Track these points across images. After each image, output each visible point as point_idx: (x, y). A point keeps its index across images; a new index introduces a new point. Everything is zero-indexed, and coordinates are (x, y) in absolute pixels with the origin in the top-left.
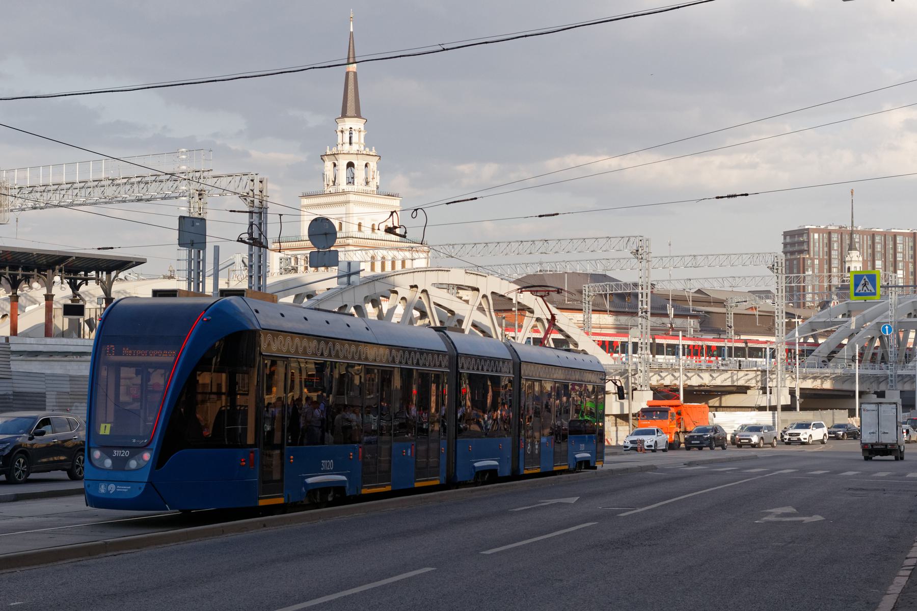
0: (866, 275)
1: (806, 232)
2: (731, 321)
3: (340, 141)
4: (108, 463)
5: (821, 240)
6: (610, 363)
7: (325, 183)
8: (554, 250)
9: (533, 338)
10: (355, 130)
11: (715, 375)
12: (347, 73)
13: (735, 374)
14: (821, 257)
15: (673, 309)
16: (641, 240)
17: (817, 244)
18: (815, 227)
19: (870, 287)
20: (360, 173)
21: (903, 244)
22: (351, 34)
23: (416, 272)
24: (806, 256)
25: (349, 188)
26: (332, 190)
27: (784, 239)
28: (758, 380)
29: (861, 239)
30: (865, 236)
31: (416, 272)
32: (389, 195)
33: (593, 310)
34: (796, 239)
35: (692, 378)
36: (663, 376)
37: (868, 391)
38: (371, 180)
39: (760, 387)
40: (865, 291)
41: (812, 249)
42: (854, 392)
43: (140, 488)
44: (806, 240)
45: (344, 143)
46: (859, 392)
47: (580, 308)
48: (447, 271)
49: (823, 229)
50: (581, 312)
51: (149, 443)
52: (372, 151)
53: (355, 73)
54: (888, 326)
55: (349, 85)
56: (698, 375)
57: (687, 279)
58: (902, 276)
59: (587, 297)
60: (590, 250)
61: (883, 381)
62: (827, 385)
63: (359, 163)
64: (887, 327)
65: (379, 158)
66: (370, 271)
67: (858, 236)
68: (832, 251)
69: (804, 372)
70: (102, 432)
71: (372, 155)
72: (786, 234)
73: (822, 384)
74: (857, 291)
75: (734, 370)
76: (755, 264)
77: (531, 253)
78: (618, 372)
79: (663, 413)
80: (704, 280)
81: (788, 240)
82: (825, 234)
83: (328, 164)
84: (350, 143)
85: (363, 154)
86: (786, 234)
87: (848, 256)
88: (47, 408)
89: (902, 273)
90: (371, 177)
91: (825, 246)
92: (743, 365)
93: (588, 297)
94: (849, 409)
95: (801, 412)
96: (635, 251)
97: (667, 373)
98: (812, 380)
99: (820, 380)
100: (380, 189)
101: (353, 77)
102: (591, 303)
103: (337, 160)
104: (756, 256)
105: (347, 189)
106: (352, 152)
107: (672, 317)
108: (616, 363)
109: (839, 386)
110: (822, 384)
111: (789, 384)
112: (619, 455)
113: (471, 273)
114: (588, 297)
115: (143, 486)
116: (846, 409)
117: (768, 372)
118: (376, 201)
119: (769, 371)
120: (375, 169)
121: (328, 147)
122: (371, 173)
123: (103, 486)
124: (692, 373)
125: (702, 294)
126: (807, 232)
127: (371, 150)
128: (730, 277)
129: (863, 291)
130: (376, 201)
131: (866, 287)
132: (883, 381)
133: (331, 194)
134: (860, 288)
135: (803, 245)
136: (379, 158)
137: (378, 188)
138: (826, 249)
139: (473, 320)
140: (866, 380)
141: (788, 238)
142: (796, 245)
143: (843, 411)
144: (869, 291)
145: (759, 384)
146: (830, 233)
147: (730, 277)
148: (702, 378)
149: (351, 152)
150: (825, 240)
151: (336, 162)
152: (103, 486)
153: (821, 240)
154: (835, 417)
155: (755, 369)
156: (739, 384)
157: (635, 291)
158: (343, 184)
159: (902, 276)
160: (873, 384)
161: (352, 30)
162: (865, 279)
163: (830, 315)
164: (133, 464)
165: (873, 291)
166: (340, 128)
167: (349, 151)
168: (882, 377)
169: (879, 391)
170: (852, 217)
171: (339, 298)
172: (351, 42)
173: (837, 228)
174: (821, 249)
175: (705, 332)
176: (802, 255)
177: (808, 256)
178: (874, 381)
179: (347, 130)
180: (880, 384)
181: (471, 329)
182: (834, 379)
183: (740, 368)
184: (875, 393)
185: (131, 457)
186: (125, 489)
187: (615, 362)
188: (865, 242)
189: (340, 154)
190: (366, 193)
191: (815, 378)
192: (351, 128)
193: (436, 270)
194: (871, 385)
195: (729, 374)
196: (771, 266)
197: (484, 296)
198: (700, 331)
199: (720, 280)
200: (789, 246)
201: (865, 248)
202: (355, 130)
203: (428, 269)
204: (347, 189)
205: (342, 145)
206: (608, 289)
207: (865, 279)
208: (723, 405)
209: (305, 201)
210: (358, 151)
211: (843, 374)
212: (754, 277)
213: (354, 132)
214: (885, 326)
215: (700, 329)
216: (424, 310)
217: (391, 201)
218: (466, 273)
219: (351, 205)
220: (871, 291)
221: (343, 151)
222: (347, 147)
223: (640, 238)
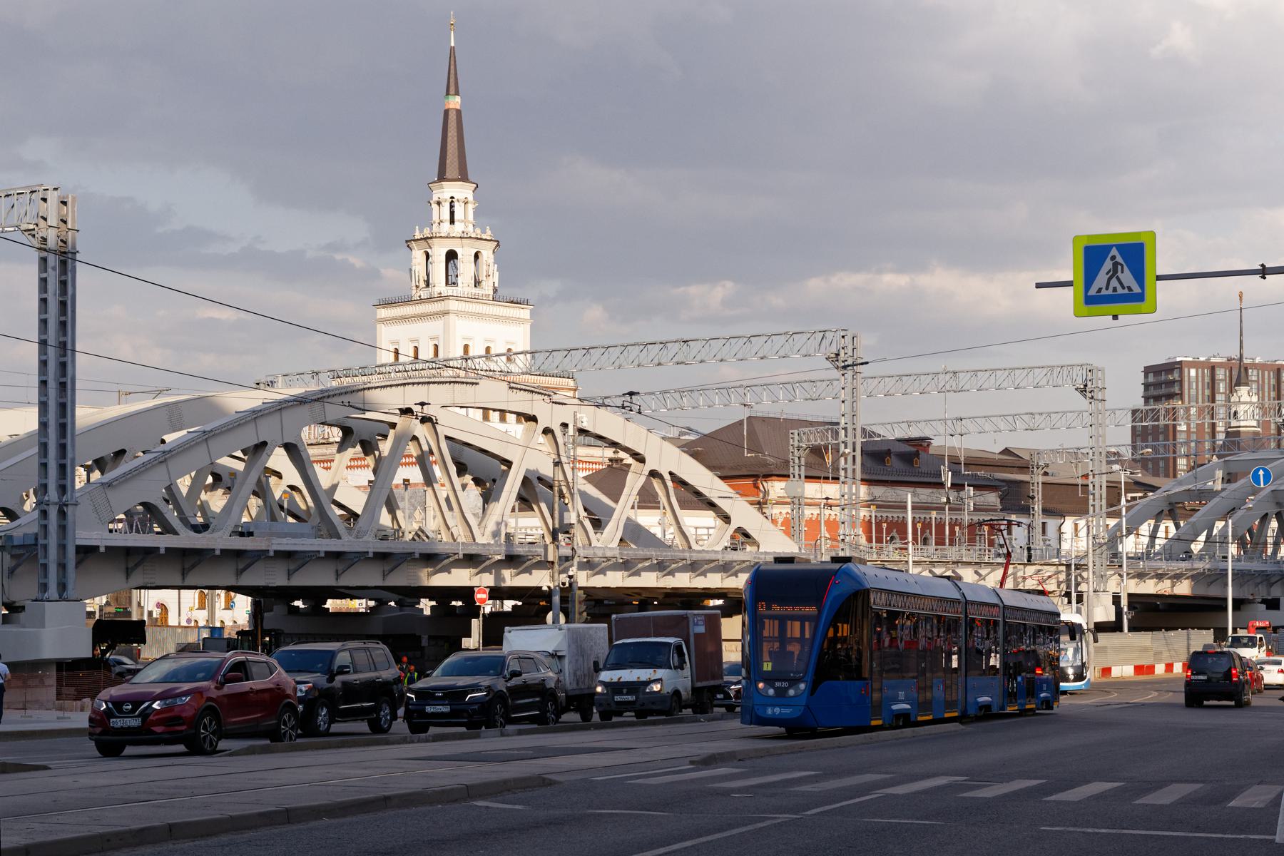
0: (1116, 246)
2: (1038, 493)
3: (435, 218)
4: (771, 692)
5: (1200, 379)
8: (699, 358)
9: (1130, 595)
10: (458, 201)
11: (983, 572)
12: (447, 112)
13: (1020, 570)
15: (950, 473)
16: (843, 337)
17: (1194, 384)
18: (1190, 359)
19: (1127, 277)
20: (465, 267)
22: (452, 49)
23: (409, 384)
24: (1177, 402)
25: (450, 291)
26: (424, 295)
28: (1061, 580)
29: (1260, 376)
30: (1266, 373)
31: (409, 384)
32: (512, 302)
33: (806, 477)
34: (1163, 378)
37: (1251, 598)
38: (484, 278)
39: (1064, 592)
40: (1115, 289)
41: (1186, 392)
42: (1226, 599)
43: (800, 710)
44: (1177, 378)
45: (442, 222)
46: (1234, 600)
47: (785, 473)
48: (473, 384)
49: (1203, 362)
51: (803, 677)
52: (485, 233)
53: (458, 112)
54: (1264, 470)
55: (449, 129)
57: (957, 419)
59: (796, 451)
60: (759, 355)
61: (1276, 582)
62: (1184, 588)
63: (465, 253)
64: (1261, 473)
65: (496, 243)
66: (482, 420)
67: (1255, 372)
68: (1217, 395)
69: (1141, 567)
70: (765, 669)
71: (486, 240)
72: (1148, 370)
73: (1173, 586)
74: (1092, 292)
75: (1019, 564)
77: (659, 364)
81: (1151, 379)
82: (1206, 370)
83: (418, 255)
84: (452, 221)
85: (470, 237)
86: (1148, 370)
87: (1235, 394)
91: (1206, 386)
93: (799, 450)
94: (1215, 629)
95: (1130, 634)
96: (833, 356)
98: (1155, 580)
100: (500, 293)
101: (455, 117)
103: (431, 248)
104: (1056, 370)
105: (446, 292)
107: (949, 486)
109: (1203, 591)
110: (1173, 586)
111: (1113, 585)
112: (688, 723)
113: (521, 390)
114: (799, 450)
115: (802, 708)
116: (1209, 629)
117: (1073, 567)
118: (491, 311)
119: (1075, 565)
120: (491, 261)
122: (485, 268)
123: (770, 709)
124: (941, 567)
125: (1010, 455)
127: (484, 232)
128: (1026, 414)
129: (1110, 292)
132: (1276, 582)
133: (421, 300)
136: (496, 243)
137: (495, 290)
138: (1207, 392)
140: (1248, 581)
141: (1151, 375)
142: (1163, 386)
143: (1204, 632)
144: (1126, 291)
145: (1063, 586)
146: (1213, 368)
147: (1026, 414)
151: (429, 251)
152: (770, 709)
153: (1200, 379)
154: (1191, 642)
155: (1055, 561)
157: (872, 439)
158: (439, 284)
160: (1260, 586)
162: (1113, 258)
163: (1196, 478)
164: (791, 692)
165: (1137, 289)
166: (435, 198)
167: (449, 234)
168: (1274, 575)
169: (1270, 598)
170: (1241, 335)
173: (1224, 360)
174: (1200, 392)
175: (1008, 512)
176: (1171, 400)
177: (1180, 402)
178: (1261, 582)
179: (446, 200)
180: (1271, 586)
182: (1193, 578)
184: (1264, 601)
185: (790, 687)
186: (788, 711)
188: (1266, 381)
189: (436, 237)
190: (474, 299)
191: (1160, 577)
192: (452, 198)
193: (450, 382)
194: (1257, 589)
196: (1082, 387)
197: (547, 431)
198: (1001, 510)
199: (1010, 419)
201: (1266, 390)
202: (458, 201)
203: (432, 380)
204: (446, 292)
207: (1113, 258)
209: (383, 313)
210: (463, 232)
211: (1209, 570)
212: (1065, 413)
213: (456, 204)
214: (1258, 470)
218: (510, 388)
219: (452, 317)
220: (1130, 289)
221: (439, 233)
222: (446, 228)
223: (843, 333)
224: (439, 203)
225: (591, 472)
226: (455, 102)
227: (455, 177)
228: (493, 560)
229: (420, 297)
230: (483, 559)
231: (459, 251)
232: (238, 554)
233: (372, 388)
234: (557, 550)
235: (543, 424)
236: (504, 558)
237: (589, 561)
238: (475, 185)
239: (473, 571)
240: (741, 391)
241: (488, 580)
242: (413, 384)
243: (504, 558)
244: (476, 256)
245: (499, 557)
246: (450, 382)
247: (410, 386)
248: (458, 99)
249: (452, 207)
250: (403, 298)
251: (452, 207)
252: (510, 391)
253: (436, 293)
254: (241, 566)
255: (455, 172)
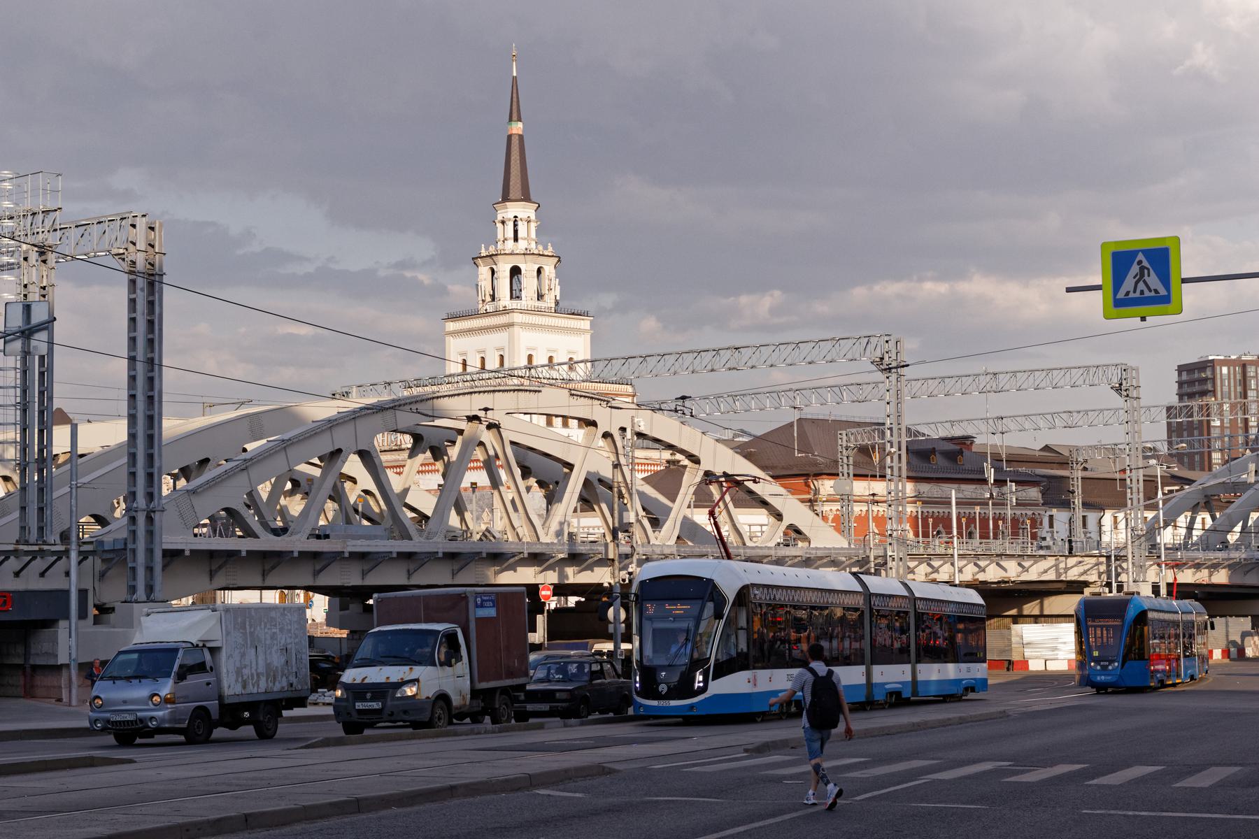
1: (1209, 364)
2: (1078, 488)
3: (500, 236)
5: (1232, 376)
6: (818, 546)
7: (480, 298)
8: (750, 364)
10: (521, 219)
12: (510, 137)
15: (993, 470)
16: (887, 342)
17: (1226, 381)
18: (1222, 358)
19: (1153, 280)
20: (529, 283)
22: (515, 79)
23: (475, 392)
25: (515, 304)
26: (490, 307)
27: (1179, 376)
31: (475, 392)
32: (573, 314)
34: (1196, 375)
35: (987, 569)
36: (982, 566)
38: (547, 292)
39: (1104, 583)
40: (1142, 292)
41: (1219, 389)
44: (1210, 376)
48: (536, 391)
49: (1234, 360)
50: (866, 478)
52: (547, 249)
53: (521, 137)
56: (998, 564)
59: (844, 451)
62: (1221, 577)
63: (528, 268)
66: (545, 425)
68: (1249, 392)
69: (1179, 557)
72: (1181, 369)
73: (1210, 576)
74: (1121, 295)
75: (1061, 556)
76: (1091, 383)
78: (853, 561)
79: (1161, 609)
80: (1024, 418)
81: (1185, 377)
82: (1237, 368)
83: (484, 271)
84: (516, 239)
85: (533, 254)
86: (1181, 369)
90: (547, 288)
92: (1077, 547)
93: (847, 449)
94: (1253, 617)
96: (878, 360)
97: (942, 562)
98: (1193, 570)
99: (1207, 571)
101: (518, 142)
102: (851, 459)
103: (496, 264)
104: (1092, 370)
106: (517, 252)
107: (992, 482)
108: (852, 546)
109: (1239, 580)
110: (1210, 576)
113: (581, 396)
114: (847, 449)
116: (1247, 616)
118: (569, 324)
119: (1115, 556)
120: (553, 275)
121: (483, 245)
126: (1211, 364)
127: (546, 248)
128: (1065, 412)
129: (1137, 294)
130: (569, 324)
131: (1145, 282)
133: (487, 314)
134: (1129, 283)
135: (1206, 384)
137: (557, 303)
138: (1239, 389)
139: (588, 472)
141: (1184, 374)
142: (1197, 383)
143: (1242, 619)
144: (1153, 294)
146: (1244, 366)
147: (1065, 412)
148: (1005, 570)
149: (515, 252)
150: (1238, 375)
151: (494, 267)
153: (1232, 376)
154: (1230, 630)
156: (1068, 579)
157: (917, 438)
161: (515, 74)
162: (1140, 262)
165: (1163, 292)
166: (500, 218)
167: (513, 251)
171: (327, 436)
172: (515, 91)
174: (1232, 389)
175: (1050, 506)
176: (1205, 397)
179: (510, 220)
181: (673, 501)
182: (1230, 567)
183: (1070, 553)
187: (849, 544)
189: (501, 254)
190: (537, 311)
191: (1198, 567)
192: (516, 217)
195: (1051, 561)
196: (1117, 385)
197: (606, 435)
198: (1043, 504)
200: (1186, 386)
202: (521, 219)
204: (510, 305)
205: (504, 242)
206: (876, 436)
207: (1140, 262)
208: (1046, 613)
209: (451, 326)
210: (526, 249)
211: (1245, 559)
212: (1102, 410)
215: (1042, 502)
217: (576, 322)
219: (516, 328)
220: (1156, 291)
221: (504, 250)
223: (887, 338)
224: (503, 222)
225: (649, 474)
226: (517, 128)
227: (518, 198)
228: (557, 559)
229: (486, 310)
230: (547, 557)
231: (523, 267)
232: (315, 555)
233: (441, 397)
234: (616, 548)
235: (602, 428)
236: (567, 556)
237: (648, 558)
238: (537, 205)
239: (537, 569)
240: (791, 394)
241: (552, 577)
242: (480, 392)
243: (567, 556)
244: (539, 271)
245: (562, 556)
246: (514, 391)
247: (477, 394)
248: (520, 125)
249: (515, 225)
250: (470, 311)
251: (515, 225)
252: (571, 398)
253: (501, 307)
254: (318, 567)
255: (518, 193)
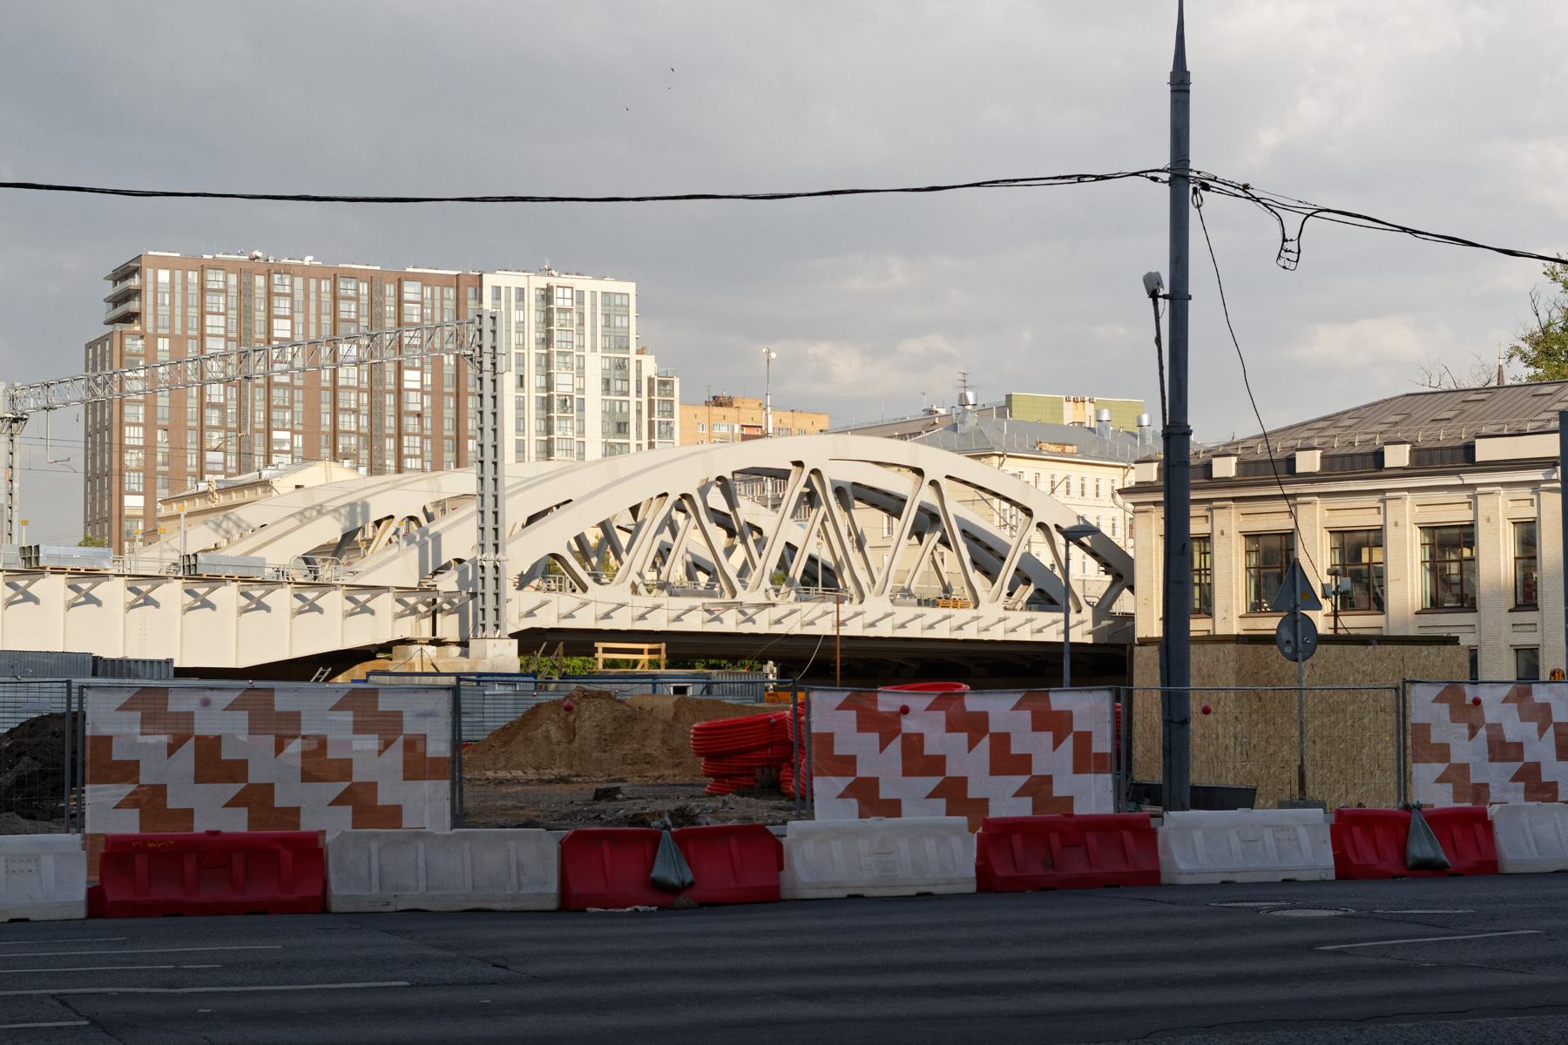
14: (178, 332)
21: (422, 303)
58: (417, 386)
88: (75, 707)
89: (419, 378)
159: (417, 386)
216: (731, 527)
